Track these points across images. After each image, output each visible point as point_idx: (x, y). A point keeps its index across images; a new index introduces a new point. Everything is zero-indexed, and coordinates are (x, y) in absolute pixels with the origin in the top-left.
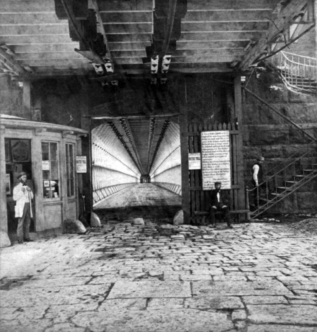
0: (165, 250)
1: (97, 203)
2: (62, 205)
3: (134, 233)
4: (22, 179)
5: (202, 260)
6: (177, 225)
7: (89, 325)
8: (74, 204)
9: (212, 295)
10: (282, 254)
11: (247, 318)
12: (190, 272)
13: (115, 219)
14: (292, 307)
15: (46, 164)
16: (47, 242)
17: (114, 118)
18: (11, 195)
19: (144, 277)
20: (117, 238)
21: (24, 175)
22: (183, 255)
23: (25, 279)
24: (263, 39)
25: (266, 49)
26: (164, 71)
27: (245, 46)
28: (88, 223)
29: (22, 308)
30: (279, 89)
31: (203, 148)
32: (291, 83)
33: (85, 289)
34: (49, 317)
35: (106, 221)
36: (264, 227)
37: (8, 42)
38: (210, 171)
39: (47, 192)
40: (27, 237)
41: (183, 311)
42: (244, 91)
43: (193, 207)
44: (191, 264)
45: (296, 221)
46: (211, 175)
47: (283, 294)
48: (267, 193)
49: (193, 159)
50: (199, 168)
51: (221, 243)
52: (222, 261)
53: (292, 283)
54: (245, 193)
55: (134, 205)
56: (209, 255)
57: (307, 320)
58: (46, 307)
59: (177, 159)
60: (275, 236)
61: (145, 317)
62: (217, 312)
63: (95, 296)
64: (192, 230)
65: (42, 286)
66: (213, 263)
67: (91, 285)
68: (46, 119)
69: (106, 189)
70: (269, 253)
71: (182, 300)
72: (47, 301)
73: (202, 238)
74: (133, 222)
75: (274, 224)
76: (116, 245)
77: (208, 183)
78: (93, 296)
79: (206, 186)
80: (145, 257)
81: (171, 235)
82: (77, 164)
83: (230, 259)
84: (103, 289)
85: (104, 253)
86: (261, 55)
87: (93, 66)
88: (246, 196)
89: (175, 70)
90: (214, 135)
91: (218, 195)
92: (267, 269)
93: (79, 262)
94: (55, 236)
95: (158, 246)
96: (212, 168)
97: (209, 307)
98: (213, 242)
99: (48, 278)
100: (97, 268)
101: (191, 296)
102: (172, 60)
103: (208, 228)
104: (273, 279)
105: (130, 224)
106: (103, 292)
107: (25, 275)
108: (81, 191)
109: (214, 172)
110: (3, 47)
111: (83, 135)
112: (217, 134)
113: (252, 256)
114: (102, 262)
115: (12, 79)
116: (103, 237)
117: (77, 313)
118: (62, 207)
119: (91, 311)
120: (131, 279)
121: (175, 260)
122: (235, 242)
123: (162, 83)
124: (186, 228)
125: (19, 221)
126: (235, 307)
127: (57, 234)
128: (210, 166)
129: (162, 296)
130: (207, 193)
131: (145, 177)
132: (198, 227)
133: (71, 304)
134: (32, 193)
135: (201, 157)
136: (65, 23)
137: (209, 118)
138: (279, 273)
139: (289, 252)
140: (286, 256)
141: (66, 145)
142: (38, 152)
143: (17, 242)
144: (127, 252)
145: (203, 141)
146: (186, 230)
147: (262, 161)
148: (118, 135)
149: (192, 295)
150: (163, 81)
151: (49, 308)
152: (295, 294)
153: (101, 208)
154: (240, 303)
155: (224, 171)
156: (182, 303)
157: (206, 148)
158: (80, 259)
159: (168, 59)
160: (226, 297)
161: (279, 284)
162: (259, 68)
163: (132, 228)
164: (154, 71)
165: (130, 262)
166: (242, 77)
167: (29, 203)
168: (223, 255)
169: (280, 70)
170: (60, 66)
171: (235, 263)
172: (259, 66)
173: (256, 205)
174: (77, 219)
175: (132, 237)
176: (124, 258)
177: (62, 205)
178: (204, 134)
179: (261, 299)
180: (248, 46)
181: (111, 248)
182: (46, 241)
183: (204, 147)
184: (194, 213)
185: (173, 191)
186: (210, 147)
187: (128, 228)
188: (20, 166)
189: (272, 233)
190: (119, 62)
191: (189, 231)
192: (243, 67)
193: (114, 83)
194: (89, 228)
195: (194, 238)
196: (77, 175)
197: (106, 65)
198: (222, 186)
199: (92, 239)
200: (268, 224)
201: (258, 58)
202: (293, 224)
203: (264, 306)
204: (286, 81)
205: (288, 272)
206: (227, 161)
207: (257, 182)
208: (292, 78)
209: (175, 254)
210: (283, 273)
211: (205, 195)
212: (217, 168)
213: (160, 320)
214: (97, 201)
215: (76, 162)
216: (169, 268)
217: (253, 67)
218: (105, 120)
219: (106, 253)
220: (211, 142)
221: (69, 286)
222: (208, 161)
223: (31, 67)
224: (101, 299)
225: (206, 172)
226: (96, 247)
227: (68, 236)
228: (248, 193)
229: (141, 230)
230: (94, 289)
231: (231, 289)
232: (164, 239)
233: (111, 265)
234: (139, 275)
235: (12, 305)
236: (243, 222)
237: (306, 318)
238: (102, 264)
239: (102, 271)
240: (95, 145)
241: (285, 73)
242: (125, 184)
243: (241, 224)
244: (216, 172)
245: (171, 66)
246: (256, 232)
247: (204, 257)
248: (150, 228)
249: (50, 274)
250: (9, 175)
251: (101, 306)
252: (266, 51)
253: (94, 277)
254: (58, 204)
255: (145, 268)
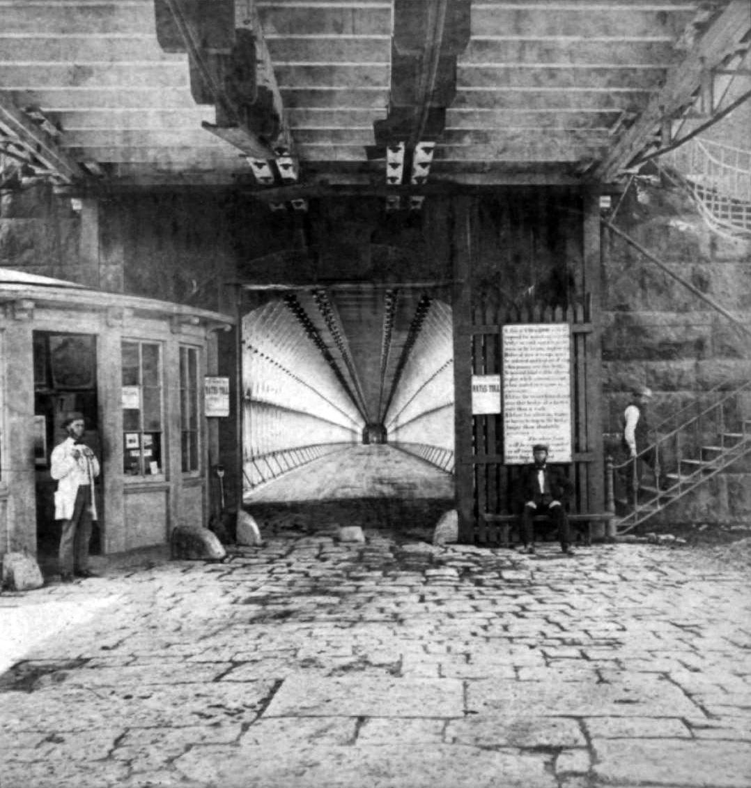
0: (411, 604)
1: (258, 489)
2: (168, 491)
3: (340, 561)
4: (72, 430)
5: (496, 630)
6: (441, 546)
7: (214, 778)
8: (198, 489)
9: (514, 712)
10: (687, 620)
11: (591, 771)
12: (464, 657)
13: (296, 528)
14: (699, 745)
15: (133, 394)
16: (129, 580)
17: (295, 288)
18: (47, 467)
19: (355, 666)
20: (299, 572)
21: (77, 418)
22: (451, 616)
23: (71, 667)
24: (653, 108)
25: (659, 134)
26: (416, 178)
27: (610, 126)
28: (230, 536)
29: (59, 735)
30: (688, 229)
31: (506, 364)
32: (716, 215)
33: (212, 691)
34: (122, 757)
35: (275, 532)
36: (647, 555)
37: (47, 105)
38: (523, 418)
39: (135, 460)
40: (83, 568)
41: (440, 750)
42: (607, 232)
43: (482, 503)
44: (469, 637)
45: (727, 541)
46: (526, 427)
47: (681, 713)
48: (658, 475)
49: (483, 389)
50: (497, 410)
51: (544, 592)
52: (543, 634)
53: (703, 689)
54: (606, 473)
55: (343, 497)
56: (514, 619)
57: (731, 777)
58: (117, 733)
59: (445, 389)
60: (675, 576)
61: (349, 762)
62: (520, 754)
63: (237, 709)
64: (478, 559)
65: (112, 684)
66: (521, 638)
67: (229, 684)
68: (135, 287)
69: (279, 457)
70: (657, 617)
71: (441, 723)
72: (121, 718)
73: (501, 577)
74: (338, 534)
75: (673, 548)
76: (295, 589)
77: (517, 447)
78: (229, 709)
79: (513, 454)
80: (361, 619)
81: (428, 568)
82: (207, 397)
83: (563, 629)
84: (255, 692)
85: (264, 609)
86: (648, 146)
87: (248, 163)
88: (606, 480)
89: (439, 177)
90: (533, 334)
91: (541, 477)
92: (648, 655)
93: (202, 630)
94: (150, 566)
95: (394, 594)
96: (528, 412)
97: (502, 741)
98: (524, 586)
99: (127, 664)
100: (243, 643)
101: (462, 714)
102: (438, 153)
103: (514, 555)
104: (661, 679)
105: (330, 540)
106: (254, 699)
107: (73, 655)
108: (215, 461)
109: (533, 421)
110: (33, 115)
111: (220, 327)
112: (541, 330)
113: (614, 622)
114: (259, 628)
115: (56, 191)
116: (265, 570)
117: (188, 748)
118: (167, 498)
119: (225, 744)
120: (323, 671)
121: (431, 628)
122: (578, 590)
123: (413, 208)
124: (464, 554)
125: (64, 528)
126: (563, 743)
127: (155, 561)
128: (523, 407)
129: (394, 714)
130: (514, 470)
131: (376, 429)
132: (493, 552)
133: (178, 727)
134: (96, 462)
135: (502, 386)
136: (180, 64)
137: (524, 293)
138: (676, 666)
139: (704, 616)
140: (696, 626)
141: (182, 350)
142: (113, 366)
143: (60, 577)
144: (320, 606)
145: (505, 346)
146: (464, 558)
147: (646, 396)
148: (311, 329)
149: (466, 712)
150: (415, 203)
151: (123, 736)
152: (708, 714)
153: (267, 501)
154: (577, 733)
155: (554, 421)
156: (439, 730)
157: (516, 365)
158: (206, 622)
159: (427, 150)
160: (544, 719)
161: (673, 691)
162: (644, 177)
163: (336, 549)
164: (393, 179)
165: (324, 630)
166: (602, 198)
167: (89, 486)
168: (546, 619)
169: (692, 185)
170: (180, 162)
171: (573, 640)
172: (642, 171)
173: (631, 502)
174: (204, 526)
175: (334, 572)
176: (312, 619)
177: (168, 491)
178: (509, 331)
179: (628, 724)
180: (618, 124)
181: (282, 597)
182: (128, 576)
183: (508, 362)
184: (482, 517)
185: (438, 463)
186: (522, 361)
187: (324, 550)
188: (70, 399)
189: (665, 569)
190: (314, 156)
191: (469, 560)
192: (605, 174)
193: (299, 204)
194: (233, 548)
195: (479, 577)
196: (206, 421)
197: (280, 162)
198: (550, 454)
199: (235, 576)
200: (658, 547)
201: (641, 153)
202: (717, 548)
203: (632, 743)
204: (706, 209)
205: (693, 660)
206: (564, 396)
207: (633, 446)
208: (720, 203)
209: (434, 613)
210: (686, 666)
211: (509, 474)
212: (541, 412)
213: (385, 769)
214: (256, 483)
215: (204, 390)
216: (416, 646)
217: (629, 175)
218: (277, 294)
219: (269, 608)
220: (526, 349)
221: (175, 684)
222: (518, 394)
223: (100, 164)
224: (249, 716)
225: (513, 421)
226: (243, 593)
227: (181, 566)
228: (611, 472)
229: (356, 555)
230: (236, 693)
231: (560, 700)
232: (411, 579)
233: (280, 635)
234: (345, 661)
235: (36, 726)
236: (599, 541)
237: (730, 773)
238: (256, 635)
239: (256, 650)
240: (259, 354)
241: (704, 192)
242: (325, 444)
243: (594, 547)
244: (537, 421)
245: (434, 167)
246: (628, 567)
247: (503, 621)
248: (377, 551)
249: (132, 655)
250: (43, 417)
251: (247, 733)
252: (659, 139)
253: (236, 664)
254: (160, 489)
255: (358, 646)
